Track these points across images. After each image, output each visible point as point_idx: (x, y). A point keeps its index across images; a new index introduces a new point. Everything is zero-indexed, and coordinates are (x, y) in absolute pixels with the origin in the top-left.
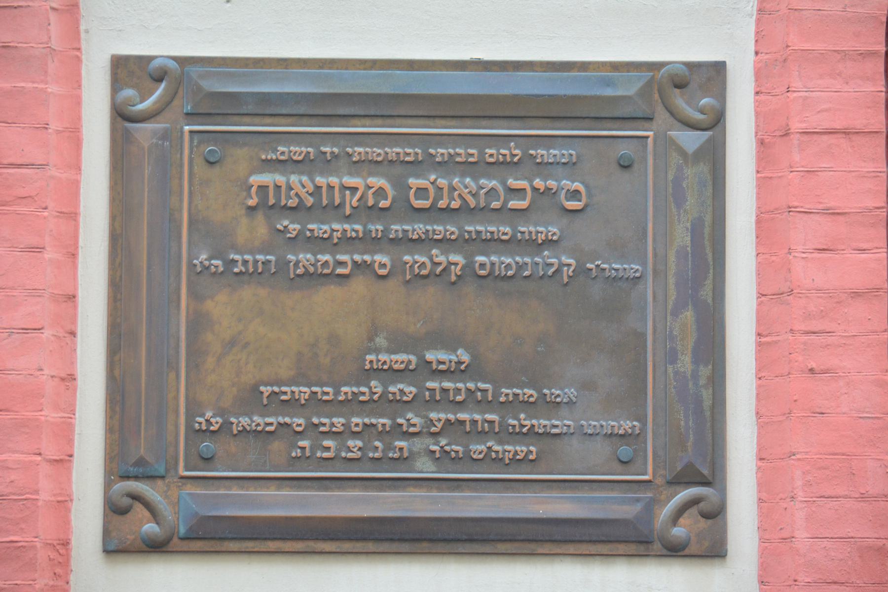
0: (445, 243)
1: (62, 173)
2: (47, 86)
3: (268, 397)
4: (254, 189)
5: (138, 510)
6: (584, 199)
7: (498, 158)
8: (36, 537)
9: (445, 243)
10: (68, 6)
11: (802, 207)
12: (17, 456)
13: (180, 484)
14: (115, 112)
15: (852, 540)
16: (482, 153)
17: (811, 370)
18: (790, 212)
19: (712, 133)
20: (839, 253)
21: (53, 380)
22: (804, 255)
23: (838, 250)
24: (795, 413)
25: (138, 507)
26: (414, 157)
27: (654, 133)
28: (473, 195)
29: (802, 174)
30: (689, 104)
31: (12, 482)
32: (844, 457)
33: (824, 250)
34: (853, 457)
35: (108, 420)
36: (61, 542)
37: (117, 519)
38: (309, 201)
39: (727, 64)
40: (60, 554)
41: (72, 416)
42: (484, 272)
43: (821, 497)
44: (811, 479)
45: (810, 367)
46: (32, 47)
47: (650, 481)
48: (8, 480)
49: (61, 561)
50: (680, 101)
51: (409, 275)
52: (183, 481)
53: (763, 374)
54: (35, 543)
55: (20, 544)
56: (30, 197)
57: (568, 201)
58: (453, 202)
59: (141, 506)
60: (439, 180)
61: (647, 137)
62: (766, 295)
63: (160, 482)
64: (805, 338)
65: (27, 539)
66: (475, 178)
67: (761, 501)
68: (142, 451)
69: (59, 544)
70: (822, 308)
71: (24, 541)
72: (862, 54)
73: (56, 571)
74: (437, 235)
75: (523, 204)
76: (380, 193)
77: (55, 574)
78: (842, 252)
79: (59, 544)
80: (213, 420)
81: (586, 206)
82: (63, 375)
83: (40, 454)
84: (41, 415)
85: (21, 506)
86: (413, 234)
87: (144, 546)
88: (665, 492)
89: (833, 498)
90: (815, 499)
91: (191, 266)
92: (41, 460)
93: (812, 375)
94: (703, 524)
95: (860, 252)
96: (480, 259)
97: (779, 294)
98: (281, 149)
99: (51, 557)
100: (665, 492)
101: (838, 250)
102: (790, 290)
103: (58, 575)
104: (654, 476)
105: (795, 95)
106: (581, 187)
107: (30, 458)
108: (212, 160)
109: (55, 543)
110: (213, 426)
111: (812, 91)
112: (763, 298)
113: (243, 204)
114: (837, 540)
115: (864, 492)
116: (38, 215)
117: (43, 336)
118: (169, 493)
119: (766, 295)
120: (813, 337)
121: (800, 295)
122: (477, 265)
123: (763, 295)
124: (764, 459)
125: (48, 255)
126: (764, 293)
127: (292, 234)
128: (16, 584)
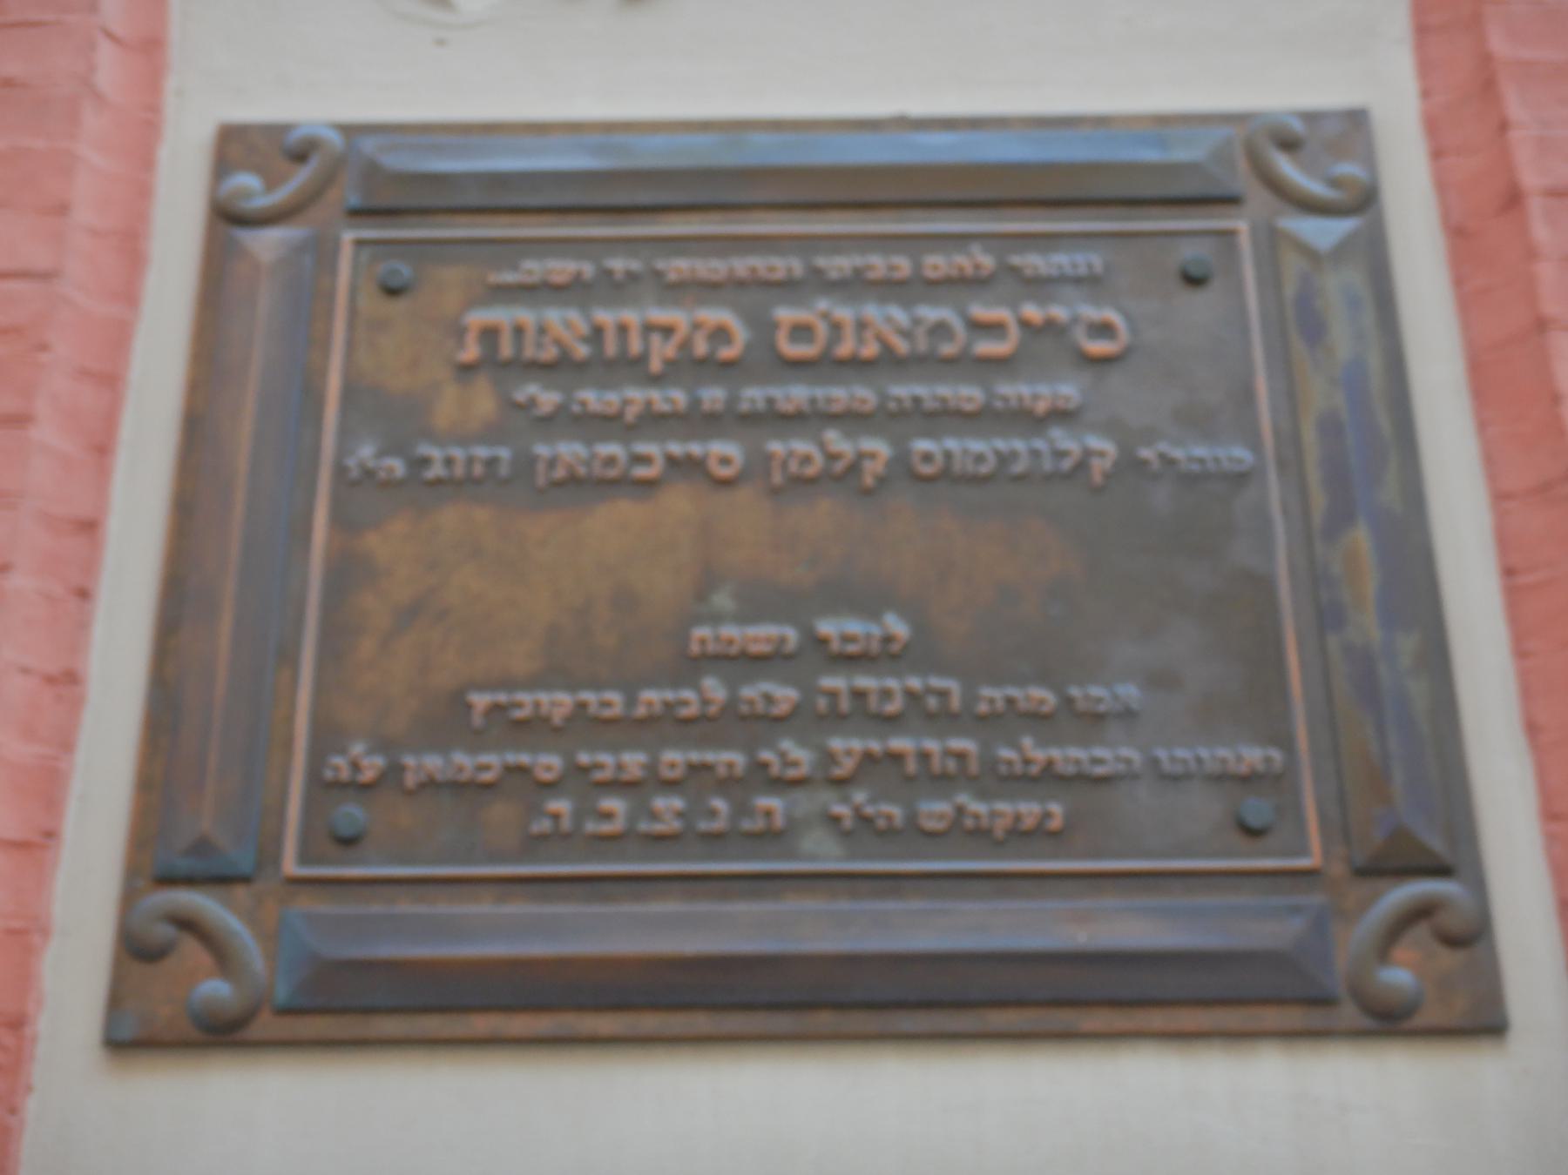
0: (852, 420)
9: (852, 420)
91: (340, 471)
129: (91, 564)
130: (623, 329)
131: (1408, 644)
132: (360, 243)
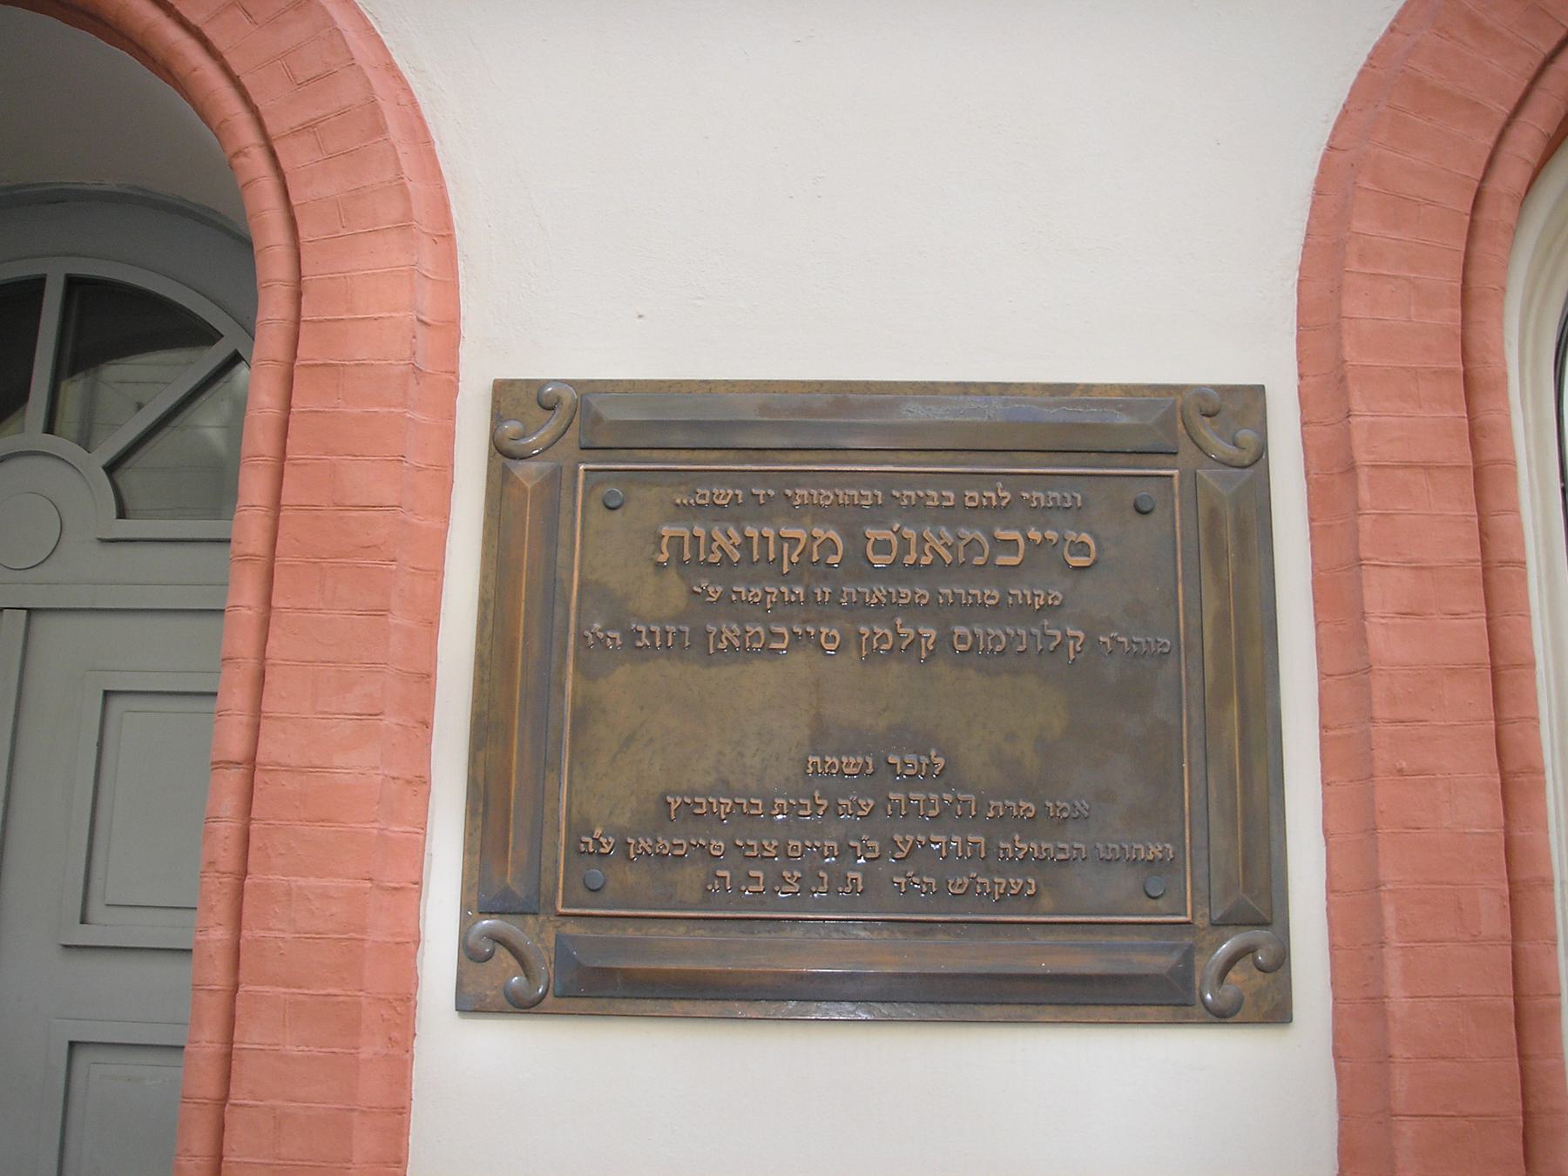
0: (913, 610)
1: (422, 520)
2: (405, 410)
3: (675, 810)
4: (665, 540)
5: (502, 956)
6: (1093, 555)
7: (981, 502)
8: (361, 990)
9: (913, 610)
10: (443, 322)
11: (1377, 559)
12: (340, 882)
13: (558, 924)
14: (493, 448)
15: (1464, 999)
16: (960, 497)
17: (1400, 772)
18: (1361, 565)
19: (1252, 471)
20: (1426, 619)
21: (395, 783)
22: (1383, 621)
23: (1425, 614)
24: (1381, 829)
25: (502, 953)
26: (871, 500)
27: (1180, 472)
28: (949, 548)
29: (1374, 517)
30: (1220, 435)
31: (332, 915)
32: (1449, 886)
33: (1408, 614)
34: (1460, 887)
35: (467, 835)
36: (400, 997)
37: (473, 965)
38: (736, 556)
39: (1266, 388)
40: (399, 1014)
41: (420, 831)
42: (964, 646)
43: (1420, 941)
44: (1406, 916)
45: (1399, 767)
46: (391, 364)
47: (1188, 923)
48: (328, 913)
49: (398, 1022)
50: (1207, 432)
51: (866, 650)
52: (561, 919)
53: (1333, 779)
54: (358, 999)
55: (341, 999)
56: (375, 546)
57: (1072, 555)
58: (924, 558)
59: (506, 951)
60: (906, 530)
61: (1171, 476)
62: (1331, 676)
63: (530, 919)
64: (1390, 728)
65: (349, 993)
66: (951, 527)
67: (1335, 947)
68: (509, 880)
69: (396, 1000)
70: (1411, 690)
71: (344, 995)
72: (1435, 372)
73: (392, 1036)
74: (903, 598)
75: (1014, 560)
76: (829, 545)
77: (390, 1039)
78: (1431, 617)
79: (396, 1000)
80: (603, 840)
81: (1095, 562)
82: (409, 777)
83: (370, 879)
84: (374, 828)
85: (344, 948)
86: (871, 598)
87: (506, 1002)
88: (1208, 937)
89: (1436, 942)
90: (1413, 944)
91: (581, 638)
92: (371, 888)
93: (1400, 778)
94: (1260, 979)
95: (1453, 617)
96: (959, 630)
97: (1349, 674)
98: (700, 491)
99: (385, 1016)
100: (1208, 937)
101: (1425, 614)
102: (1367, 666)
103: (395, 1042)
104: (1193, 917)
105: (1359, 419)
106: (722, 845)
107: (358, 885)
108: (610, 505)
109: (391, 998)
110: (603, 847)
111: (1378, 416)
112: (1329, 680)
113: (652, 559)
114: (1444, 999)
115: (1476, 933)
116: (383, 569)
117: (381, 723)
118: (543, 936)
119: (1331, 676)
120: (1400, 727)
121: (1382, 672)
122: (955, 637)
123: (1328, 675)
124: (1337, 891)
125: (388, 721)
126: (1329, 673)
127: (713, 597)
128: (334, 1052)
129: (429, 705)
130: (764, 539)
131: (704, 385)
132: (586, 470)
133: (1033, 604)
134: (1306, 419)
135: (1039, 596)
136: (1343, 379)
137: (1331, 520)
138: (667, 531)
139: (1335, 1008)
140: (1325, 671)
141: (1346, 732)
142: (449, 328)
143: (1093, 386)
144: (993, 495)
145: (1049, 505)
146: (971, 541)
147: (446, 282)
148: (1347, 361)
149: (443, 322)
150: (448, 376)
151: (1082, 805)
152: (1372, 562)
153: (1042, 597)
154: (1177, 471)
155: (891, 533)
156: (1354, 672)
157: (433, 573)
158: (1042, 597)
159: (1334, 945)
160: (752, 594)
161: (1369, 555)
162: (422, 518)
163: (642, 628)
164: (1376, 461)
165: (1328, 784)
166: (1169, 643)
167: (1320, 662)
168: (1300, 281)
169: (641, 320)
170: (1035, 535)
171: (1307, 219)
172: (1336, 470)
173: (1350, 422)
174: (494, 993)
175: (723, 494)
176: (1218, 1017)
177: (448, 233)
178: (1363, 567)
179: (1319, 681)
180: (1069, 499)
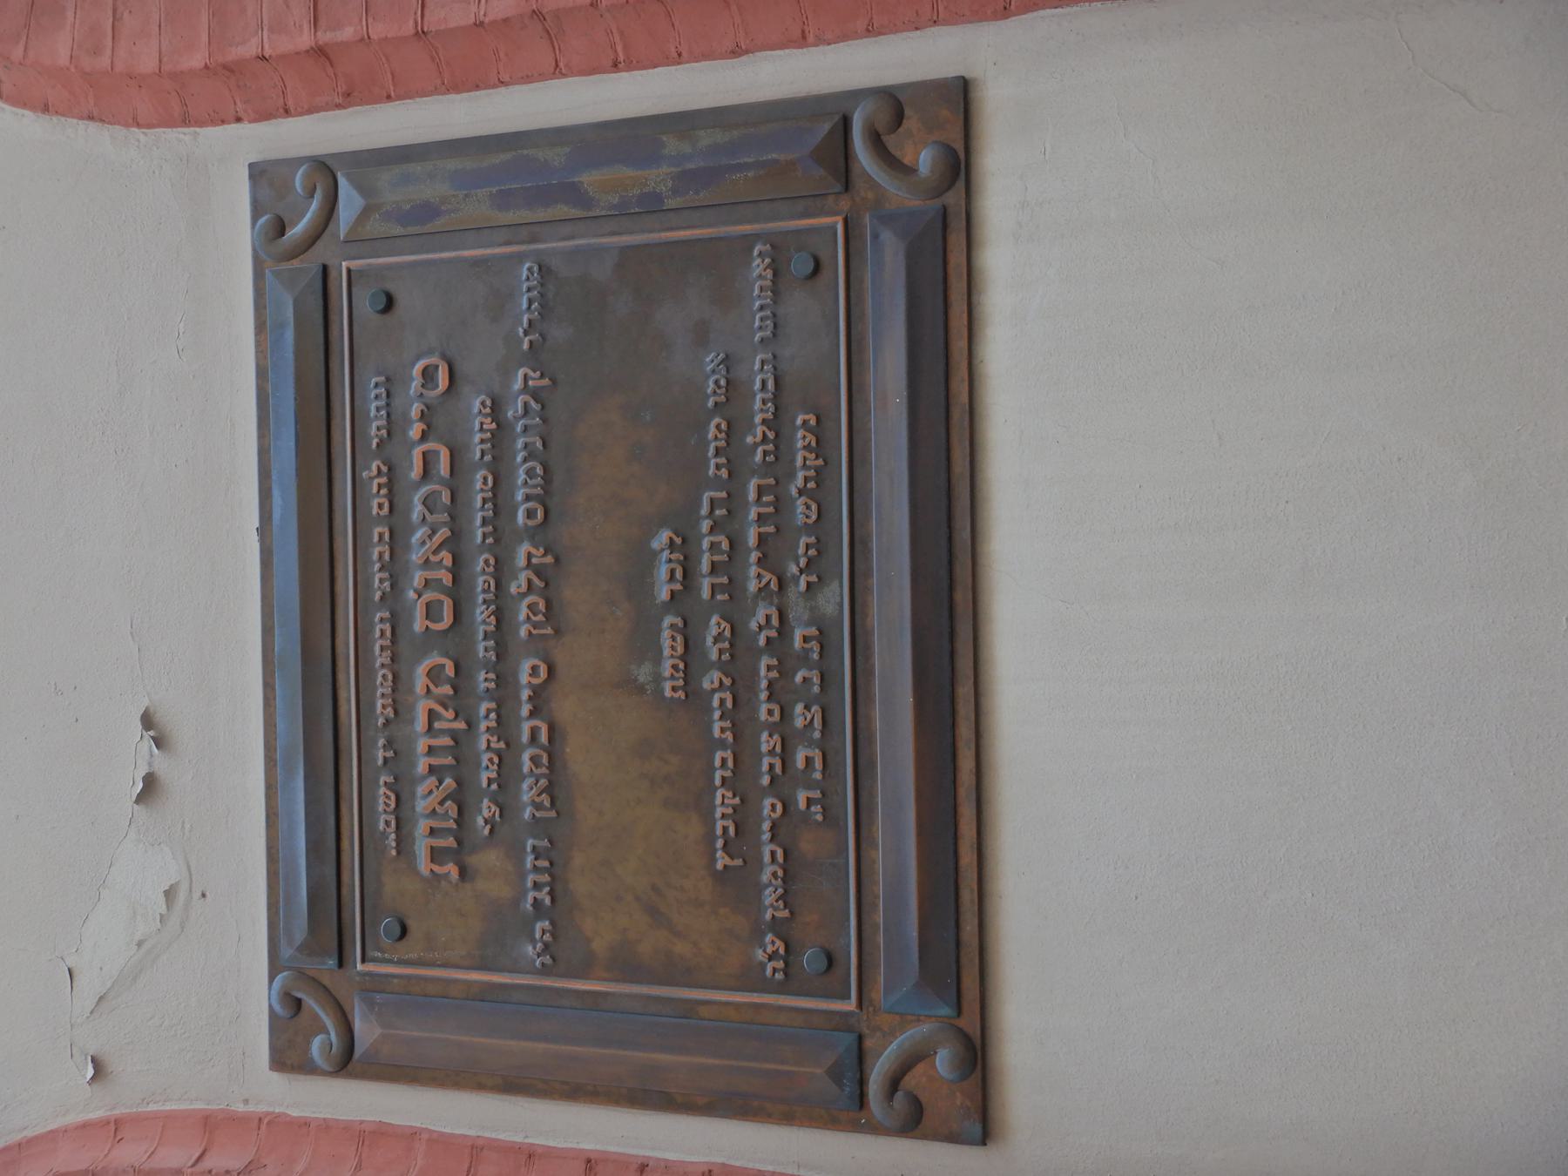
1: (416, 1164)
4: (436, 868)
10: (205, 1132)
11: (416, 13)
13: (871, 1009)
18: (423, 32)
28: (434, 532)
29: (370, 20)
47: (846, 221)
53: (673, 50)
57: (437, 386)
59: (907, 1078)
61: (349, 271)
67: (871, 29)
80: (770, 949)
86: (490, 624)
91: (545, 971)
94: (911, 122)
102: (535, 17)
104: (835, 214)
105: (266, 46)
123: (557, 66)
124: (803, 32)
132: (363, 960)
133: (490, 431)
134: (281, 110)
135: (482, 424)
136: (225, 67)
137: (386, 72)
138: (424, 865)
139: (947, 23)
140: (553, 70)
141: (617, 39)
142: (211, 1125)
143: (258, 366)
144: (376, 482)
145: (385, 416)
146: (425, 506)
147: (163, 1126)
148: (206, 64)
149: (205, 1132)
150: (263, 1127)
151: (713, 361)
152: (419, 19)
153: (484, 420)
154: (344, 263)
155: (420, 600)
156: (548, 32)
157: (475, 1152)
158: (484, 420)
159: (868, 30)
160: (490, 765)
161: (411, 23)
162: (414, 1162)
163: (531, 895)
164: (310, 21)
165: (680, 55)
166: (527, 265)
167: (542, 77)
168: (139, 126)
169: (208, 894)
170: (415, 431)
171: (75, 121)
172: (330, 71)
173: (270, 56)
174: (958, 1094)
175: (383, 799)
176: (958, 174)
177: (112, 1125)
178: (425, 30)
179: (565, 76)
180: (377, 391)
